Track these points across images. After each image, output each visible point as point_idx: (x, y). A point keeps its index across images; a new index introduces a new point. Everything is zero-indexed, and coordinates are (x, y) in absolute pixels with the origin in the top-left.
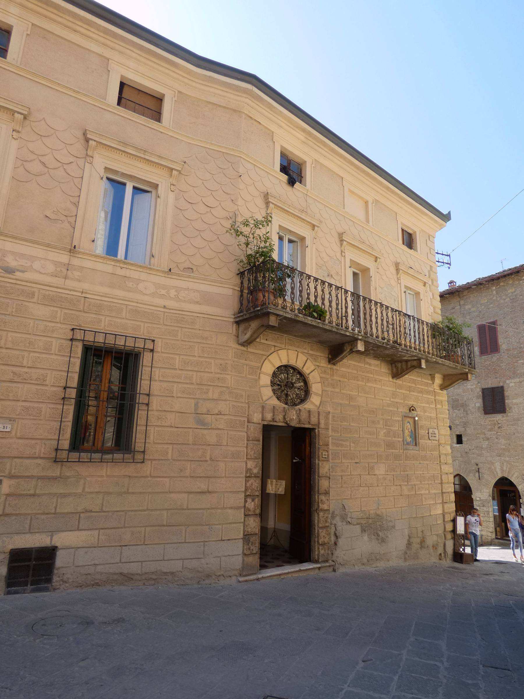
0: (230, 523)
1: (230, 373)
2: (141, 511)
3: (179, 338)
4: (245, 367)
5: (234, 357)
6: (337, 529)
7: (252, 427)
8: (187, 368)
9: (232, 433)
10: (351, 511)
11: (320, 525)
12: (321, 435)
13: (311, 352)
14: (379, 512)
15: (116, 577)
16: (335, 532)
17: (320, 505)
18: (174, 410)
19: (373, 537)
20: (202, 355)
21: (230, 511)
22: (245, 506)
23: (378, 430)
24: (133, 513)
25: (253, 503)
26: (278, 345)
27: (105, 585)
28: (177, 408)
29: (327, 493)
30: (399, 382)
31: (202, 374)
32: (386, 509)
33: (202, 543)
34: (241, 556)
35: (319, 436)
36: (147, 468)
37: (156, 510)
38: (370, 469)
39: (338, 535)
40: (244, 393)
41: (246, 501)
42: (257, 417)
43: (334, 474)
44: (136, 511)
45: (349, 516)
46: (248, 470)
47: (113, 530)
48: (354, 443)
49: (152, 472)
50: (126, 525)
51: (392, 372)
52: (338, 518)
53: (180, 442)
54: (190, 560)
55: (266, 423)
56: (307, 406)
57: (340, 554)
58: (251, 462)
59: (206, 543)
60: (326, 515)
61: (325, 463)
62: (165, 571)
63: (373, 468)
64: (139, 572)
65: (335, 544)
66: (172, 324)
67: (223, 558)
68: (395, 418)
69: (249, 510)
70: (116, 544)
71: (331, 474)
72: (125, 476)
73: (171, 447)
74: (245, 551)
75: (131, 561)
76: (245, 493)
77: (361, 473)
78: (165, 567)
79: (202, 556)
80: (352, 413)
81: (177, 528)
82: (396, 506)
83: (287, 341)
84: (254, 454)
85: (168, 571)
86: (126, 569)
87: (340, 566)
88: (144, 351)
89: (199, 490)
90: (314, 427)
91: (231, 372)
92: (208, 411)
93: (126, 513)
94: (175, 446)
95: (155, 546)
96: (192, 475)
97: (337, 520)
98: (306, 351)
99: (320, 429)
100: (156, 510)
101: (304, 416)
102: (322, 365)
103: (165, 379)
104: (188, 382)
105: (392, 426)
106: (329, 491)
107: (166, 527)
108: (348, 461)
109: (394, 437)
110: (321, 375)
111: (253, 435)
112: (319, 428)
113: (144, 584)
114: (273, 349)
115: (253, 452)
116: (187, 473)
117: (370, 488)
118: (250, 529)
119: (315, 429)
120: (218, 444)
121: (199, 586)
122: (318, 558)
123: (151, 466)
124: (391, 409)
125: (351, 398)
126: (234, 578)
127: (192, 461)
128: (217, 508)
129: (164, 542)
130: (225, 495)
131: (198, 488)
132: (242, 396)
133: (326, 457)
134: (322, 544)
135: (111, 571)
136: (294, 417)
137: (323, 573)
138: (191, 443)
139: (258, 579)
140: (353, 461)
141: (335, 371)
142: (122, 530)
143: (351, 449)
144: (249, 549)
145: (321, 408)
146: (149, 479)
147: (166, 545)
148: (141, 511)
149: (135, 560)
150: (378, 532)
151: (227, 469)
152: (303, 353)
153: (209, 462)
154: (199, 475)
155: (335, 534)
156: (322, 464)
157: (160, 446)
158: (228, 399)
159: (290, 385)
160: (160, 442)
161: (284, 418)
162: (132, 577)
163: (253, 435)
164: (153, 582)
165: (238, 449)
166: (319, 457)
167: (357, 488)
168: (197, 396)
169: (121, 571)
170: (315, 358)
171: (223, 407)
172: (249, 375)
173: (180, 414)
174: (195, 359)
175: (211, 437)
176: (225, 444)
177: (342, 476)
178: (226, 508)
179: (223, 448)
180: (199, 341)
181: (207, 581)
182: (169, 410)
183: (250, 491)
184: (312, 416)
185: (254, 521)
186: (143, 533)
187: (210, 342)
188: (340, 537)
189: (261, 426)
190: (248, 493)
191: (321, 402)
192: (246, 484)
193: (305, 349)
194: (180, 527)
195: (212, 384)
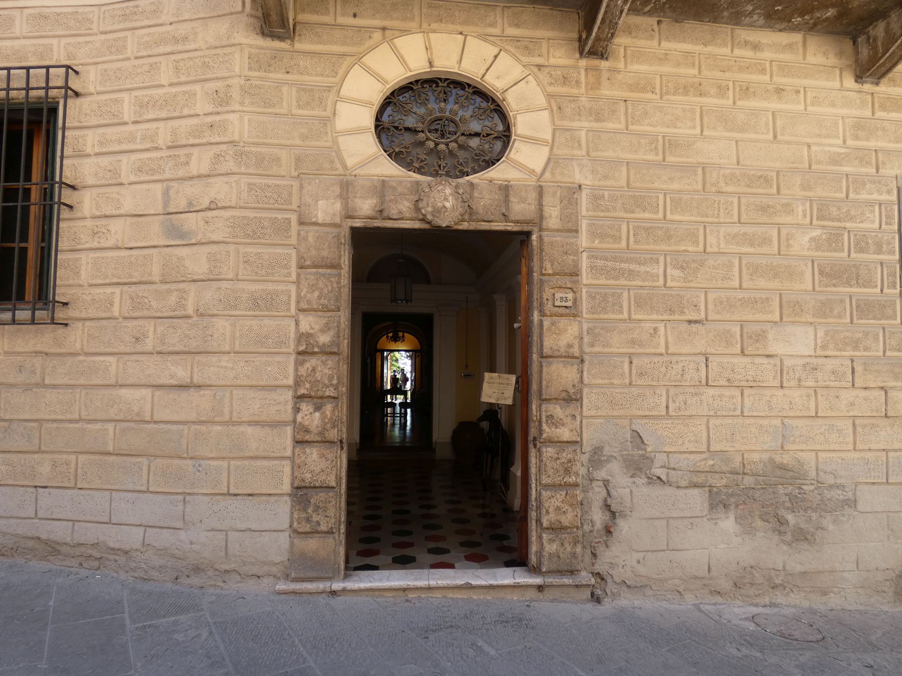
0: (251, 458)
1: (237, 107)
2: (70, 421)
3: (129, 54)
4: (285, 89)
5: (250, 69)
6: (613, 492)
7: (312, 234)
8: (146, 117)
9: (250, 249)
10: (667, 449)
11: (545, 480)
12: (547, 249)
13: (511, 31)
14: (786, 459)
15: (31, 544)
16: (605, 500)
17: (545, 427)
18: (122, 212)
19: (759, 523)
20: (175, 80)
21: (250, 430)
22: (294, 421)
23: (784, 232)
24: (55, 425)
25: (317, 414)
26: (396, 24)
27: (12, 556)
28: (128, 206)
29: (572, 398)
30: (884, 88)
31: (176, 123)
32: (817, 451)
33: (181, 497)
34: (287, 534)
35: (542, 250)
36: (76, 337)
37: (96, 421)
38: (751, 341)
39: (614, 508)
40: (283, 154)
41: (297, 410)
42: (327, 209)
43: (597, 349)
44: (61, 421)
45: (657, 464)
46: (302, 337)
47: (20, 455)
48: (682, 268)
49: (85, 343)
50: (43, 448)
51: (857, 61)
52: (615, 467)
53: (134, 280)
54: (158, 530)
55: (358, 224)
56: (499, 173)
57: (621, 558)
58: (311, 318)
59: (188, 498)
60: (566, 455)
61: (563, 322)
62: (112, 545)
63: (760, 337)
64: (68, 540)
65: (608, 532)
66: (117, 27)
67: (233, 536)
68: (864, 196)
69: (307, 431)
70: (27, 483)
71: (587, 350)
72: (37, 353)
73: (117, 290)
74: (295, 524)
75: (54, 517)
76: (296, 391)
77: (709, 351)
78: (113, 537)
79: (179, 524)
80: (675, 186)
81: (134, 460)
82: (859, 446)
83: (424, 11)
84: (319, 298)
85: (117, 546)
86: (46, 530)
87: (624, 588)
88: (66, 97)
89: (173, 382)
90: (526, 228)
91: (242, 103)
92: (190, 204)
93: (41, 426)
94: (126, 288)
95: (94, 493)
96: (158, 349)
97: (615, 472)
98: (496, 31)
99: (544, 233)
100: (96, 421)
101: (484, 200)
102: (552, 61)
103: (104, 150)
104: (148, 146)
105: (852, 219)
106: (581, 392)
107: (114, 457)
108: (654, 317)
109: (861, 250)
110: (551, 89)
111: (314, 252)
112: (541, 230)
113: (81, 564)
114: (377, 36)
115: (316, 294)
116: (149, 344)
117: (747, 392)
118: (308, 476)
119: (528, 234)
120: (212, 277)
121: (175, 588)
122: (540, 563)
123: (83, 330)
124: (847, 169)
125: (671, 144)
126: (266, 581)
127: (159, 318)
128: (214, 423)
129: (110, 487)
130: (235, 392)
131: (172, 377)
132: (278, 159)
133: (569, 304)
134: (548, 529)
135: (20, 531)
136: (446, 203)
137: (552, 601)
138: (157, 279)
139: (334, 593)
140: (677, 317)
141: (605, 75)
142: (36, 456)
143: (669, 284)
144: (308, 520)
145: (547, 175)
146: (81, 358)
147: (114, 493)
148: (70, 421)
149: (61, 517)
150: (782, 512)
151: (237, 335)
152: (484, 37)
153: (195, 318)
154: (171, 349)
155: (607, 507)
156: (553, 324)
157: (98, 290)
158: (235, 169)
159: (441, 127)
160: (100, 282)
161: (418, 209)
162: (57, 547)
163: (314, 252)
164: (96, 564)
165: (270, 287)
166: (541, 304)
167: (692, 390)
168: (167, 175)
169: (38, 535)
170: (527, 47)
171: (219, 190)
172: (299, 107)
173: (136, 219)
174: (161, 91)
175: (196, 262)
176: (231, 276)
177: (630, 356)
178: (240, 423)
179: (224, 285)
180: (168, 49)
181: (196, 581)
182: (115, 212)
183: (308, 386)
184: (512, 199)
185: (322, 456)
186: (73, 466)
187: (193, 46)
188: (624, 516)
189: (346, 233)
190: (302, 391)
191: (549, 160)
192: (296, 370)
193: (493, 25)
194: (139, 459)
195: (197, 141)
